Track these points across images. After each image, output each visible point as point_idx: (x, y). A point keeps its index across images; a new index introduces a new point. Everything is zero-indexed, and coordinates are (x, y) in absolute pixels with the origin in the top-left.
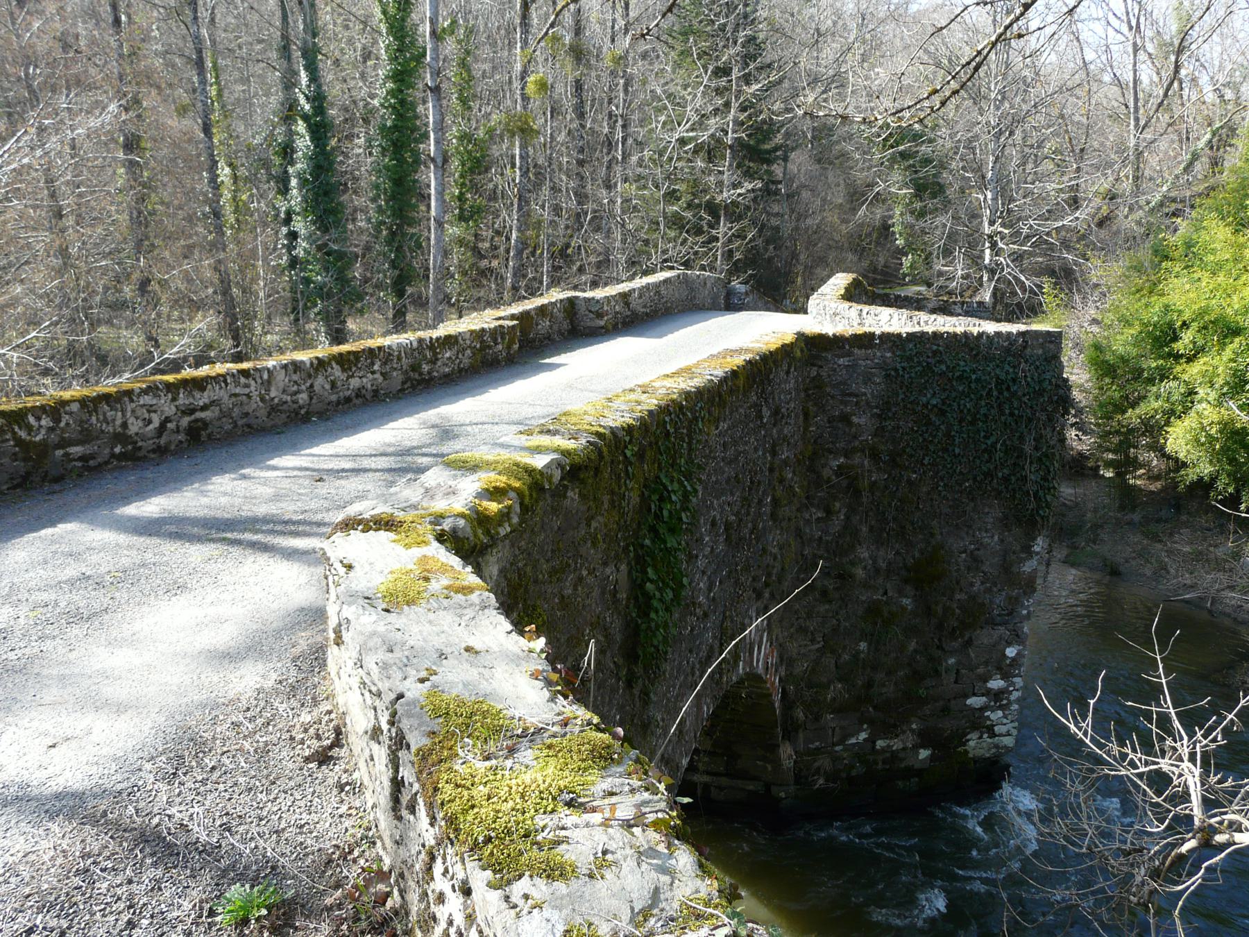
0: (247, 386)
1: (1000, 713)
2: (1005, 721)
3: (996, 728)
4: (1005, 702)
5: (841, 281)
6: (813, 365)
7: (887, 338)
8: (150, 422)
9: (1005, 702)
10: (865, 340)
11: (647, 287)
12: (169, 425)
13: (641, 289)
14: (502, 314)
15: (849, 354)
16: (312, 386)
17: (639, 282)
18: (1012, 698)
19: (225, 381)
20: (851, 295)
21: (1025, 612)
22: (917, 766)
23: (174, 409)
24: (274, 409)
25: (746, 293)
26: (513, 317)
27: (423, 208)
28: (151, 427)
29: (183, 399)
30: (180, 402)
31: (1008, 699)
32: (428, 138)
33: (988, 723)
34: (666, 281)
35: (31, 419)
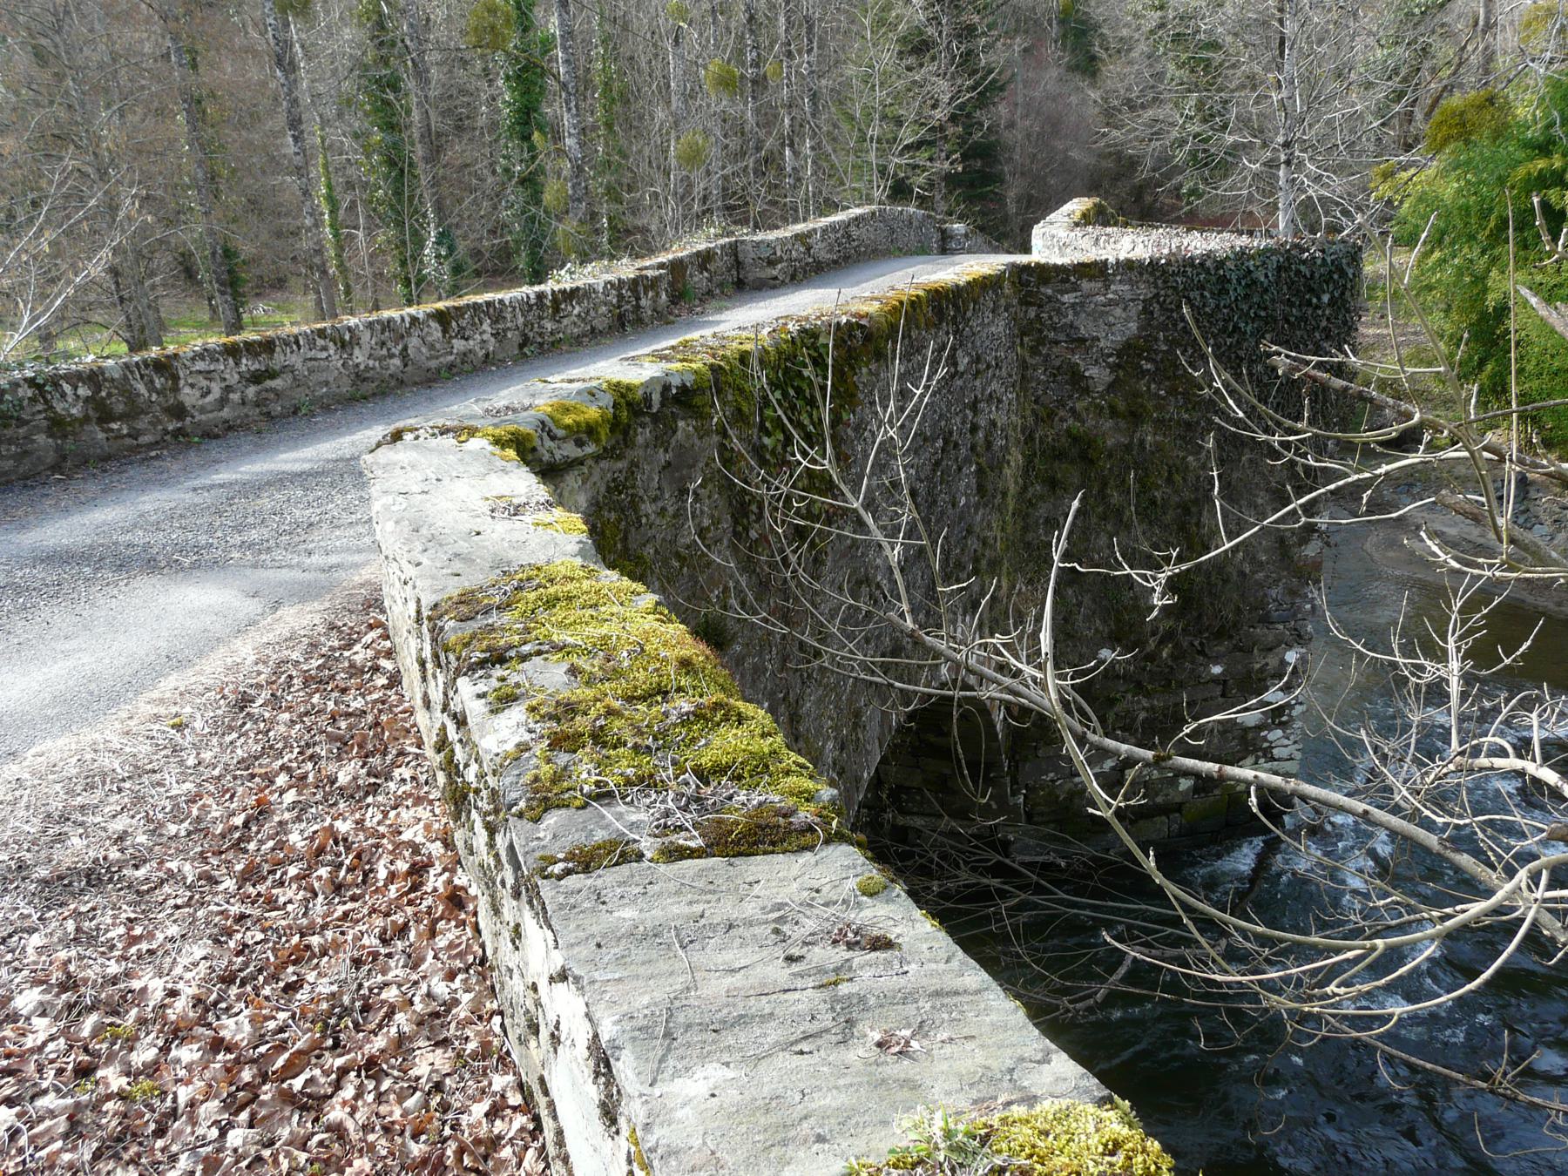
0: (324, 349)
1: (1279, 733)
2: (1286, 742)
3: (1275, 751)
4: (1284, 719)
5: (1077, 206)
6: (1031, 304)
7: (1129, 265)
8: (208, 392)
9: (1284, 719)
10: (1096, 270)
11: (833, 228)
12: (231, 396)
13: (825, 230)
14: (648, 263)
15: (1075, 288)
16: (405, 348)
17: (825, 221)
18: (1294, 713)
19: (297, 342)
20: (1086, 220)
21: (1308, 606)
22: (1178, 799)
23: (237, 377)
24: (360, 377)
25: (966, 235)
26: (661, 266)
27: (1339, 819)
28: (210, 398)
29: (247, 364)
30: (243, 368)
31: (1289, 715)
32: (678, 157)
33: (1265, 745)
34: (857, 220)
35: (67, 388)
